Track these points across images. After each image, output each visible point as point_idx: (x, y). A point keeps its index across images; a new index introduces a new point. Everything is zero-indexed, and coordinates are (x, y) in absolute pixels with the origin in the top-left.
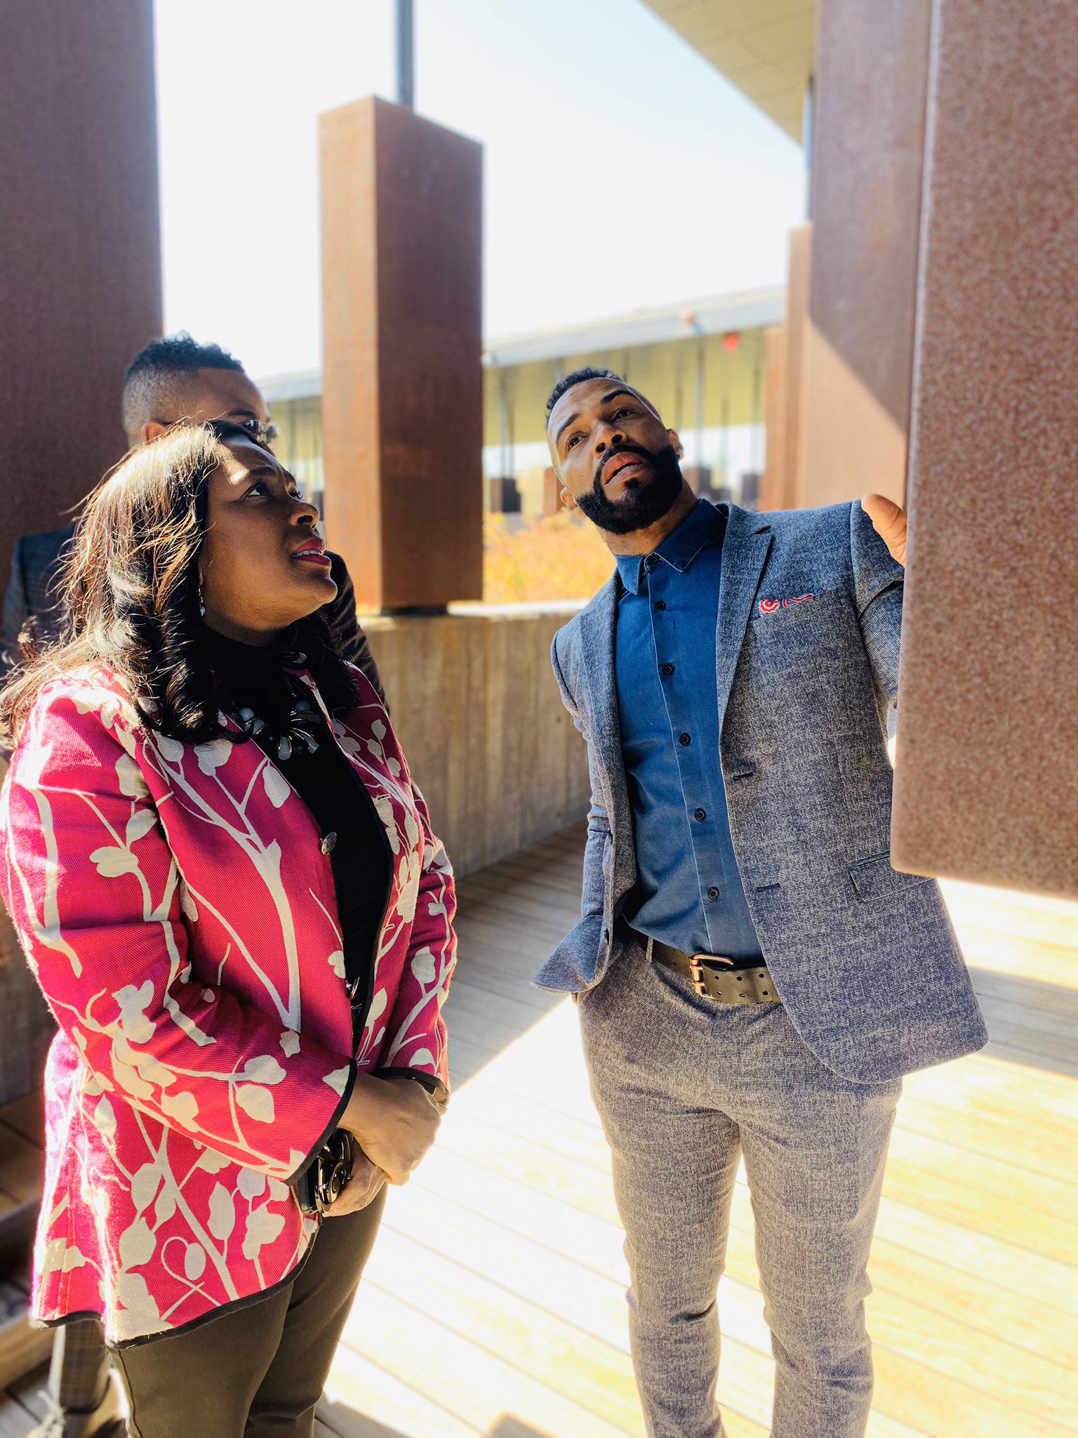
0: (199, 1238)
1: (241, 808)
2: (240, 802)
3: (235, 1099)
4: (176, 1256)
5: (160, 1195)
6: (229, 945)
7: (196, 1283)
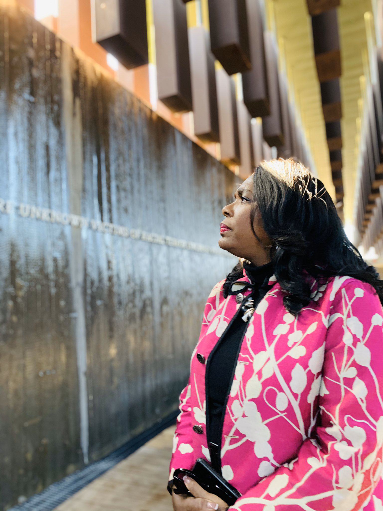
0: (285, 390)
4: (272, 397)
5: (265, 366)
7: (282, 412)
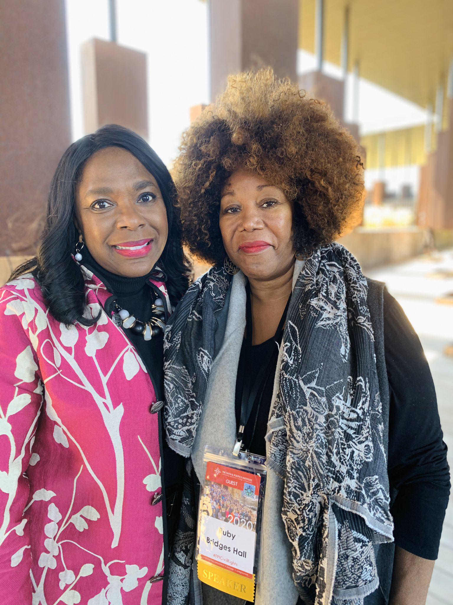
1: (105, 380)
2: (105, 375)
3: (125, 353)
6: (82, 466)
